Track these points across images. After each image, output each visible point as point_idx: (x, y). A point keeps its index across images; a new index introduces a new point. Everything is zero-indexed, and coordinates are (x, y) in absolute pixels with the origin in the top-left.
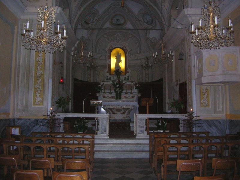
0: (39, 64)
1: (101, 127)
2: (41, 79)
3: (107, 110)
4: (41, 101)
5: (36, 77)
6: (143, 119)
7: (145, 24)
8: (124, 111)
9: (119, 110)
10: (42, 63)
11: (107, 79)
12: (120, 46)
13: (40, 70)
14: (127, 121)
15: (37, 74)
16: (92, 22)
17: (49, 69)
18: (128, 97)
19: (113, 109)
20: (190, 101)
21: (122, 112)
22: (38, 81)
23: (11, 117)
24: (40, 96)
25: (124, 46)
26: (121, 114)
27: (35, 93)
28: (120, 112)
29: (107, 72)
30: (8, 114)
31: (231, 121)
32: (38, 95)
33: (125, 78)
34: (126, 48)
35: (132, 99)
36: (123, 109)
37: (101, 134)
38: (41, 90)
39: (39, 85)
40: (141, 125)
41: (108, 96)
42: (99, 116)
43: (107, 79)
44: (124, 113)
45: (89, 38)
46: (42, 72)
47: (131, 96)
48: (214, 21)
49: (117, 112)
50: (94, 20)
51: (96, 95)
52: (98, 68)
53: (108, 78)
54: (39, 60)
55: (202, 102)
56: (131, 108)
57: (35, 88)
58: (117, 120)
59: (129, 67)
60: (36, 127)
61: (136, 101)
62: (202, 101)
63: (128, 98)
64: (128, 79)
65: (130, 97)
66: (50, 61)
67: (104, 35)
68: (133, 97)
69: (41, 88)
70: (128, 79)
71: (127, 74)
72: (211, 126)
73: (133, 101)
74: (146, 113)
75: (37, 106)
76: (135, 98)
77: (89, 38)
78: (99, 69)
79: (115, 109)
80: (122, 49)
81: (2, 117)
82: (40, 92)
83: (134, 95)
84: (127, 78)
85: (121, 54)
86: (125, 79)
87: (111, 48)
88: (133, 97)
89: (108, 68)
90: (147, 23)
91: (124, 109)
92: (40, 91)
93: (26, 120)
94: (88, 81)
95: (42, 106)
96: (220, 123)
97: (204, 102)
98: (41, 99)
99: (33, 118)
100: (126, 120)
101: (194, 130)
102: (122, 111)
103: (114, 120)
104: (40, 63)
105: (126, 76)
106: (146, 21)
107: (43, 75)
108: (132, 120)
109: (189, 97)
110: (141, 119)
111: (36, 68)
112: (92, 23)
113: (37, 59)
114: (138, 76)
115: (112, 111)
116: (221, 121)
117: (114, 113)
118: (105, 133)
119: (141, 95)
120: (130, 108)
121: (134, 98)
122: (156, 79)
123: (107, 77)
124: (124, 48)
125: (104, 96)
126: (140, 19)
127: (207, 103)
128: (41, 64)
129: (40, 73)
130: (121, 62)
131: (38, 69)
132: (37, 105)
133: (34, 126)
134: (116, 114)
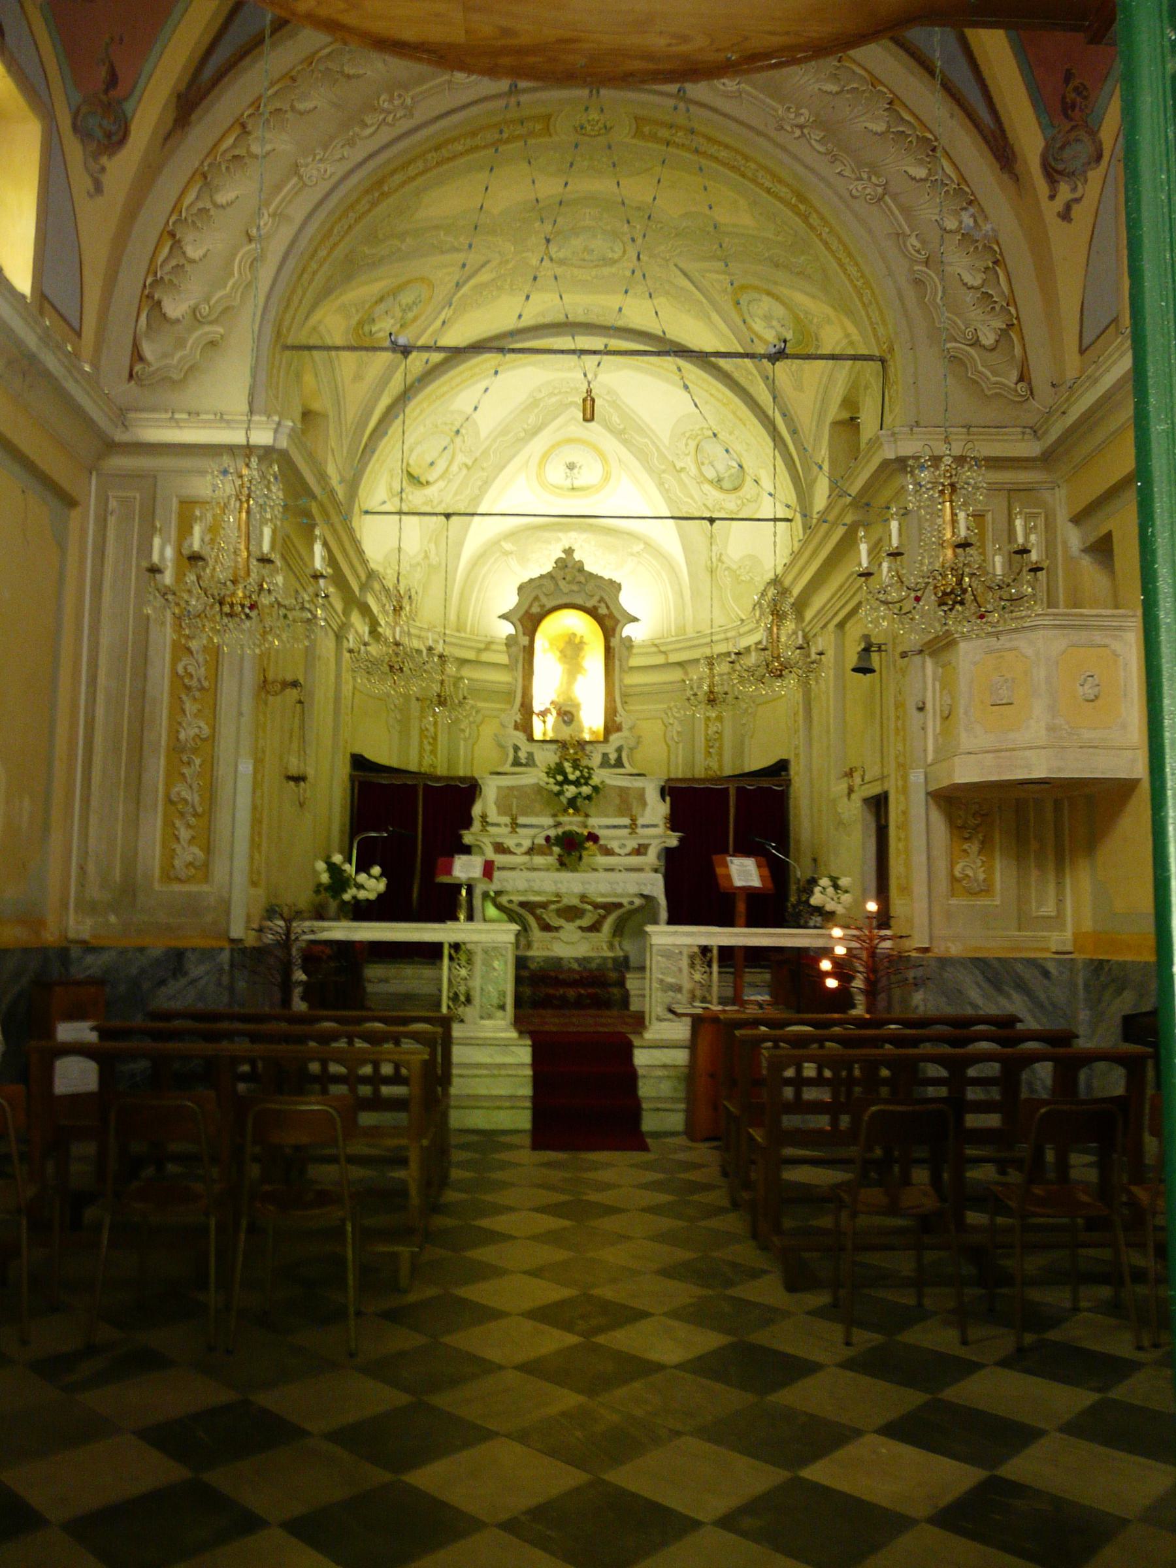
0: (188, 688)
1: (482, 989)
2: (198, 762)
3: (512, 910)
4: (197, 863)
5: (177, 749)
6: (681, 953)
7: (707, 487)
8: (596, 917)
9: (571, 913)
10: (206, 684)
11: (517, 763)
12: (579, 601)
13: (196, 716)
14: (610, 964)
15: (182, 736)
16: (441, 477)
17: (241, 714)
18: (617, 850)
19: (544, 905)
20: (902, 870)
21: (586, 922)
22: (185, 770)
23: (50, 936)
24: (193, 838)
25: (601, 600)
26: (580, 928)
27: (168, 824)
28: (579, 923)
29: (516, 728)
30: (36, 923)
31: (1098, 967)
32: (184, 834)
33: (605, 756)
34: (608, 608)
35: (635, 860)
36: (589, 907)
37: (482, 1018)
38: (200, 810)
39: (191, 787)
40: (670, 980)
41: (519, 845)
42: (475, 937)
43: (517, 763)
44: (595, 928)
45: (426, 557)
46: (202, 724)
47: (632, 844)
48: (954, 521)
49: (561, 922)
50: (454, 468)
51: (460, 837)
52: (472, 707)
53: (522, 755)
54: (191, 669)
55: (957, 874)
56: (632, 903)
57: (169, 801)
58: (561, 959)
59: (624, 703)
60: (173, 987)
61: (656, 871)
62: (958, 869)
63: (620, 855)
64: (619, 763)
65: (628, 850)
66: (241, 669)
67: (503, 544)
68: (640, 850)
69: (197, 799)
70: (619, 763)
71: (613, 737)
72: (1000, 990)
73: (639, 870)
74: (721, 948)
75: (177, 887)
76: (652, 857)
77: (426, 557)
78: (477, 712)
79: (553, 907)
80: (592, 612)
81: (11, 935)
82: (193, 821)
83: (646, 842)
84: (613, 757)
85: (585, 640)
86: (605, 763)
87: (535, 609)
88: (640, 850)
89: (522, 705)
90: (718, 483)
91: (596, 906)
92: (196, 815)
93: (122, 952)
94: (423, 770)
95: (206, 888)
96: (1046, 974)
97: (970, 873)
98: (201, 855)
99: (157, 946)
100: (605, 959)
101: (917, 1007)
102: (589, 915)
103: (547, 960)
104: (194, 683)
105: (610, 749)
106: (711, 474)
107: (212, 739)
108: (633, 962)
109: (897, 849)
110: (668, 954)
111: (177, 708)
112: (441, 484)
113: (183, 663)
114: (668, 746)
115: (539, 919)
116: (1052, 968)
117: (547, 928)
118: (500, 1014)
119: (681, 840)
120: (625, 901)
121: (645, 854)
122: (757, 761)
123: (516, 749)
124: (603, 611)
125: (501, 844)
126: (679, 465)
127: (981, 876)
128: (202, 689)
129: (197, 730)
130: (516, 722)
131: (183, 711)
132: (180, 881)
133: (162, 982)
134: (557, 929)
